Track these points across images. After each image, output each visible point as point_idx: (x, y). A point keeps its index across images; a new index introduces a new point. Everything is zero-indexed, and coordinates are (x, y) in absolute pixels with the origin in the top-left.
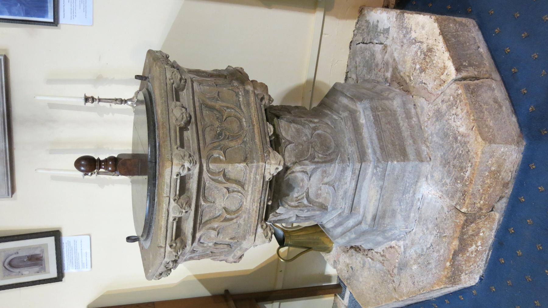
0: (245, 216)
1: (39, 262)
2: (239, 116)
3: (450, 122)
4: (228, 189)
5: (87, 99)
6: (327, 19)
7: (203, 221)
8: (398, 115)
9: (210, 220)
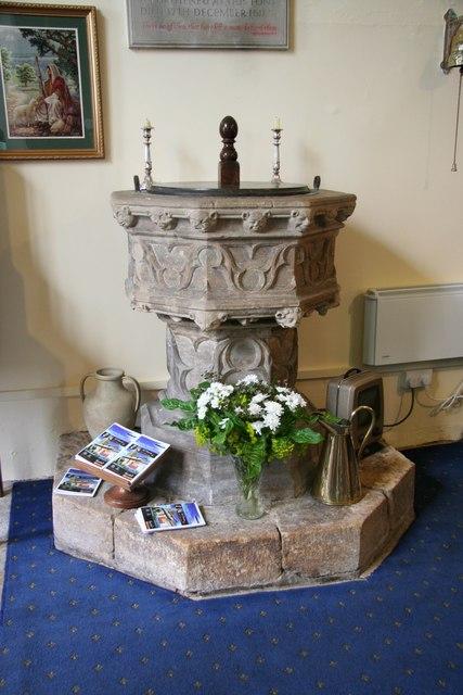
5: (278, 131)
6: (385, 423)
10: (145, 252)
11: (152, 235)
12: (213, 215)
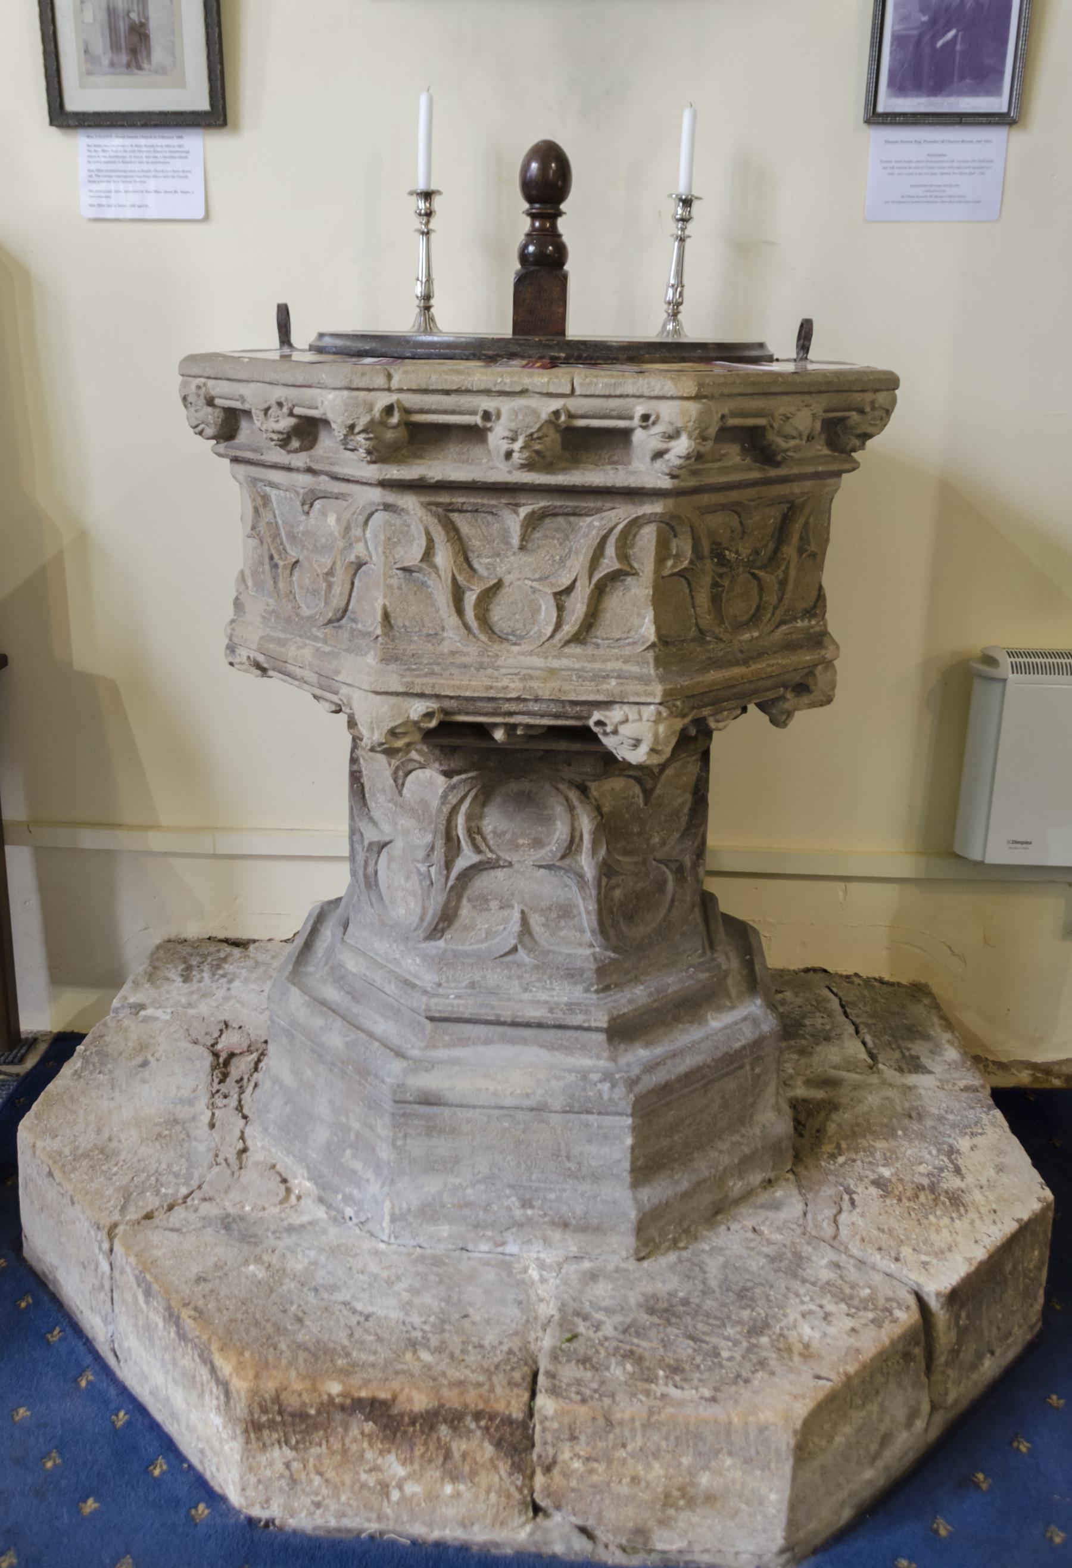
0: (471, 652)
1: (124, 58)
2: (765, 619)
3: (793, 1300)
4: (569, 590)
7: (455, 516)
8: (743, 1131)
9: (460, 539)
10: (256, 510)
11: (785, 480)
12: (389, 410)
